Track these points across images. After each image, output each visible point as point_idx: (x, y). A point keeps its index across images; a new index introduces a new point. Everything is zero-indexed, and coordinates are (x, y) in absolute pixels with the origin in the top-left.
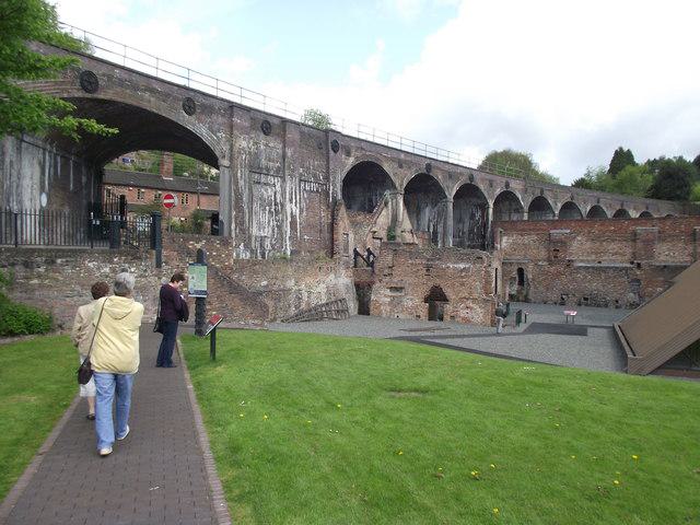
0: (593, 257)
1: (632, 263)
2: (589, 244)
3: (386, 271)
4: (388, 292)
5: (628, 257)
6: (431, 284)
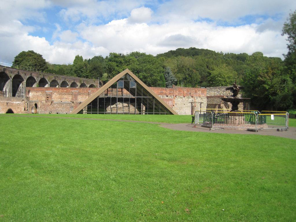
1: (71, 101)
6: (8, 108)
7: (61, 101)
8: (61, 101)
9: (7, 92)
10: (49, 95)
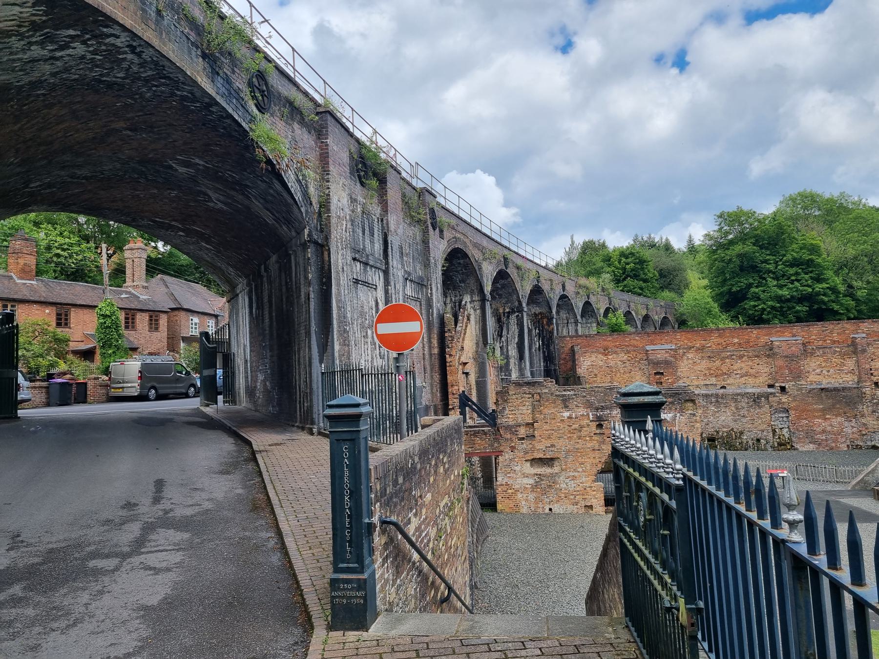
0: (713, 380)
2: (704, 364)
3: (522, 431)
4: (528, 468)
5: (763, 379)
7: (723, 387)
8: (723, 387)
9: (512, 361)
10: (667, 363)
